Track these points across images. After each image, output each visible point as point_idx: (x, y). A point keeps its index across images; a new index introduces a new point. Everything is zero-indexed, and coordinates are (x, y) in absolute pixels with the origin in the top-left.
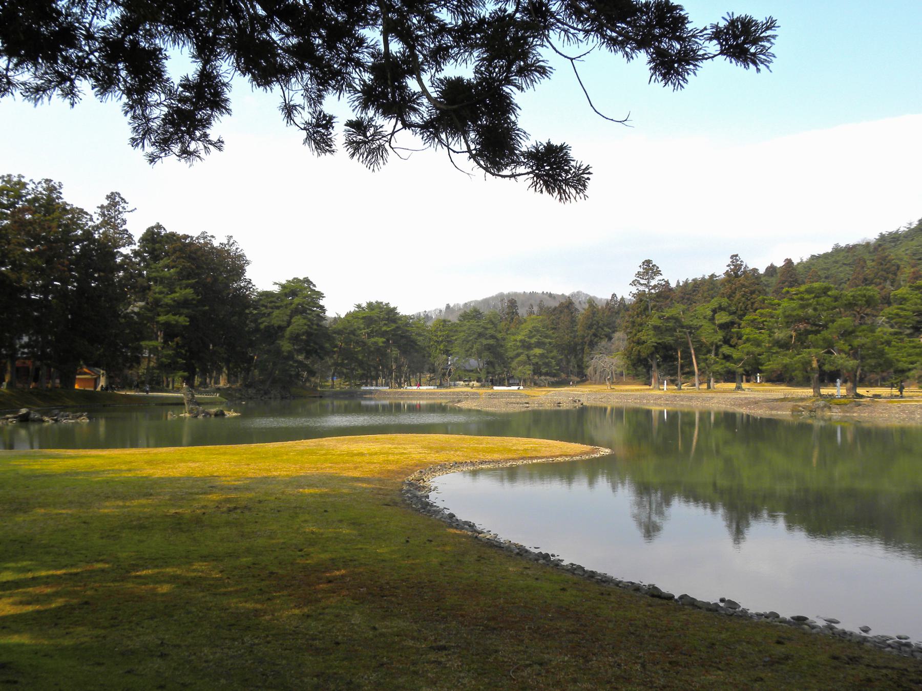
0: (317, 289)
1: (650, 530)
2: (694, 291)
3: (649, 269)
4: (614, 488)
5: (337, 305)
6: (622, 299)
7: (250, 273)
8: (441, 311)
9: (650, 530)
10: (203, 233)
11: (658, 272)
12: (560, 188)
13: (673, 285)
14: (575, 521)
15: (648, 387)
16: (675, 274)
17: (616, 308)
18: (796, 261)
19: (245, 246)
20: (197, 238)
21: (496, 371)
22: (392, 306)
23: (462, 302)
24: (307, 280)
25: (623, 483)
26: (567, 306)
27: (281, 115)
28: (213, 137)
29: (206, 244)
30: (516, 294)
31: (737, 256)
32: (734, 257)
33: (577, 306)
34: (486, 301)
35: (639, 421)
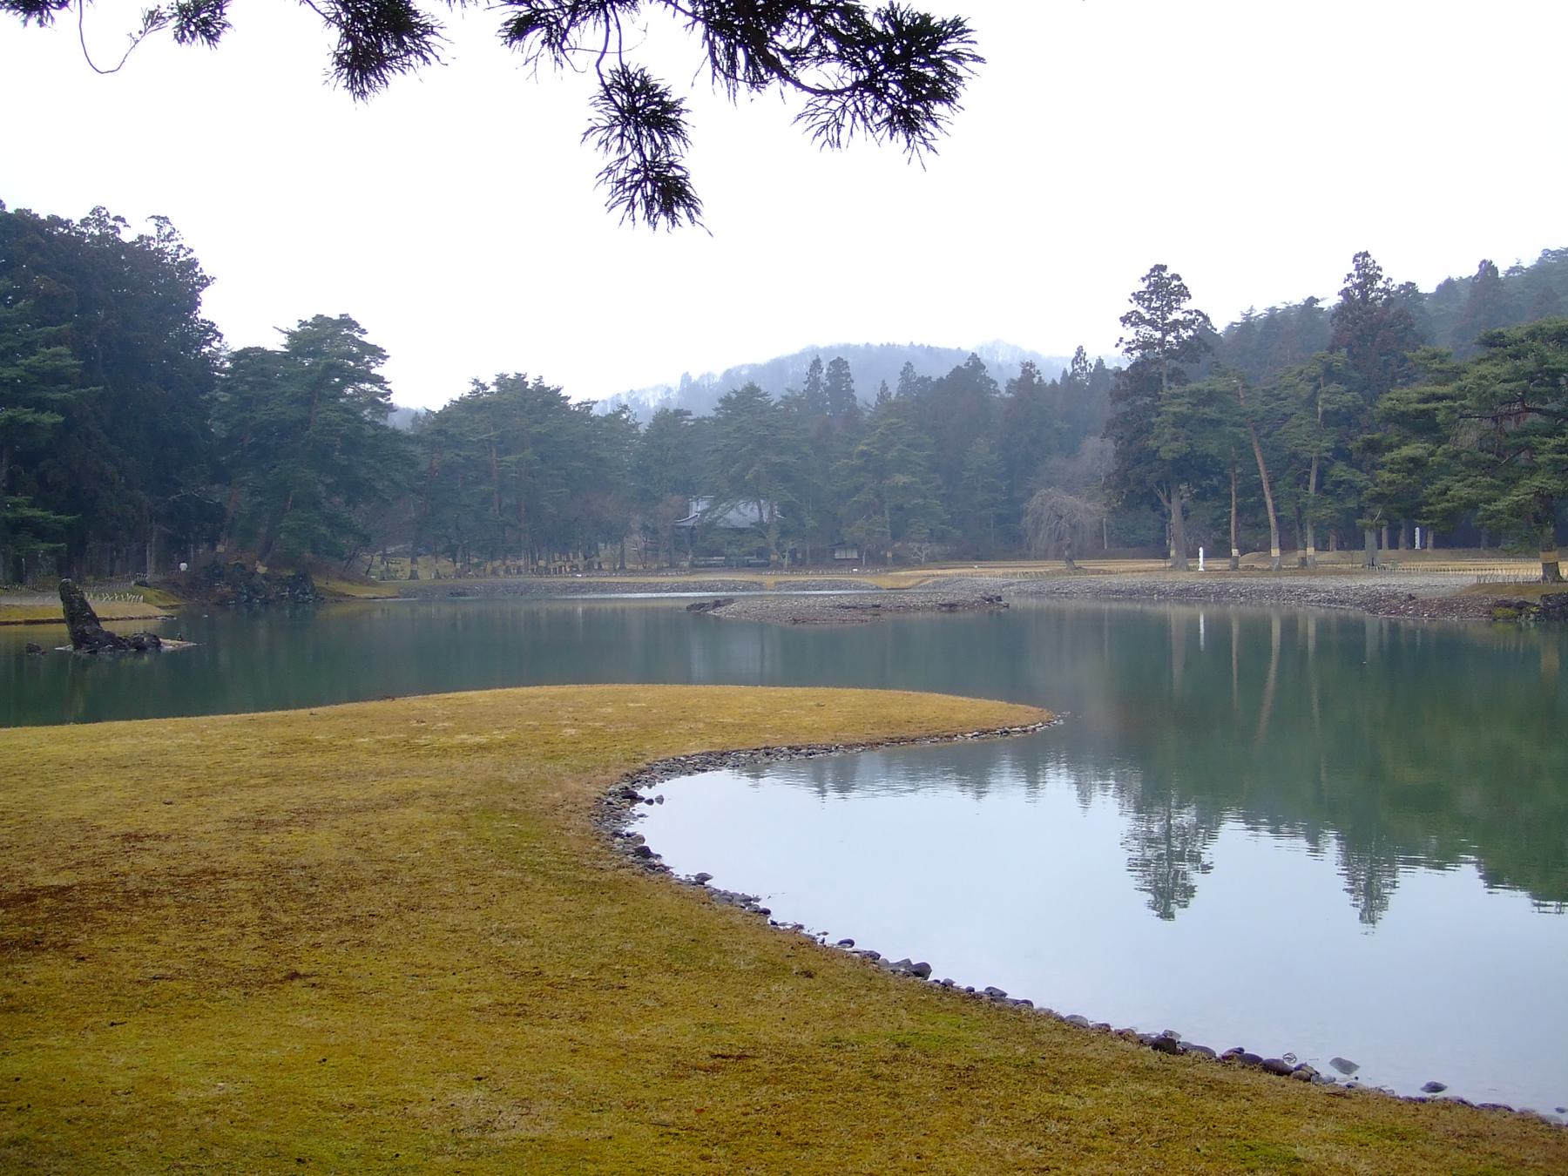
0: (364, 338)
1: (1168, 893)
2: (1271, 333)
3: (1163, 288)
4: (1084, 797)
5: (422, 379)
6: (1100, 362)
7: (210, 307)
8: (669, 390)
9: (1168, 893)
10: (95, 211)
11: (1183, 292)
12: (897, 25)
13: (1220, 324)
14: (997, 883)
15: (1161, 564)
16: (1223, 300)
17: (1085, 383)
18: (1502, 268)
19: (202, 240)
20: (85, 223)
21: (811, 537)
22: (563, 393)
23: (718, 371)
24: (347, 322)
25: (1105, 788)
26: (969, 376)
27: (1561, 1106)
28: (1206, 859)
29: (103, 238)
30: (846, 348)
31: (1366, 255)
32: (1362, 259)
33: (991, 373)
34: (778, 366)
35: (1137, 640)
